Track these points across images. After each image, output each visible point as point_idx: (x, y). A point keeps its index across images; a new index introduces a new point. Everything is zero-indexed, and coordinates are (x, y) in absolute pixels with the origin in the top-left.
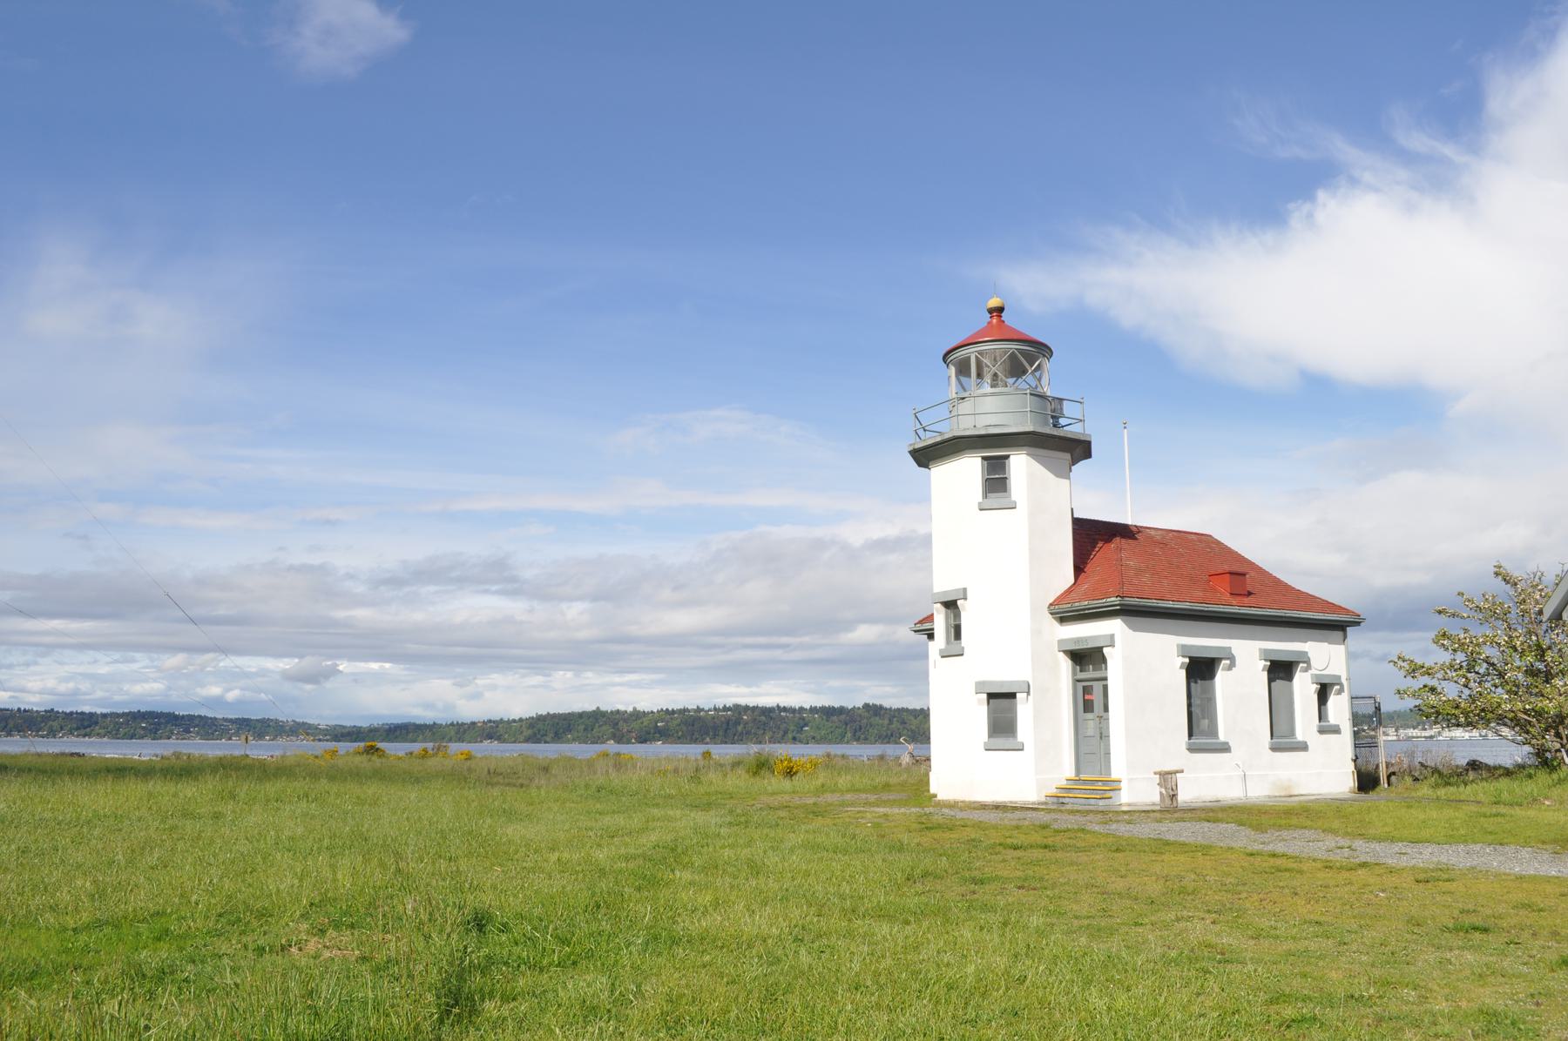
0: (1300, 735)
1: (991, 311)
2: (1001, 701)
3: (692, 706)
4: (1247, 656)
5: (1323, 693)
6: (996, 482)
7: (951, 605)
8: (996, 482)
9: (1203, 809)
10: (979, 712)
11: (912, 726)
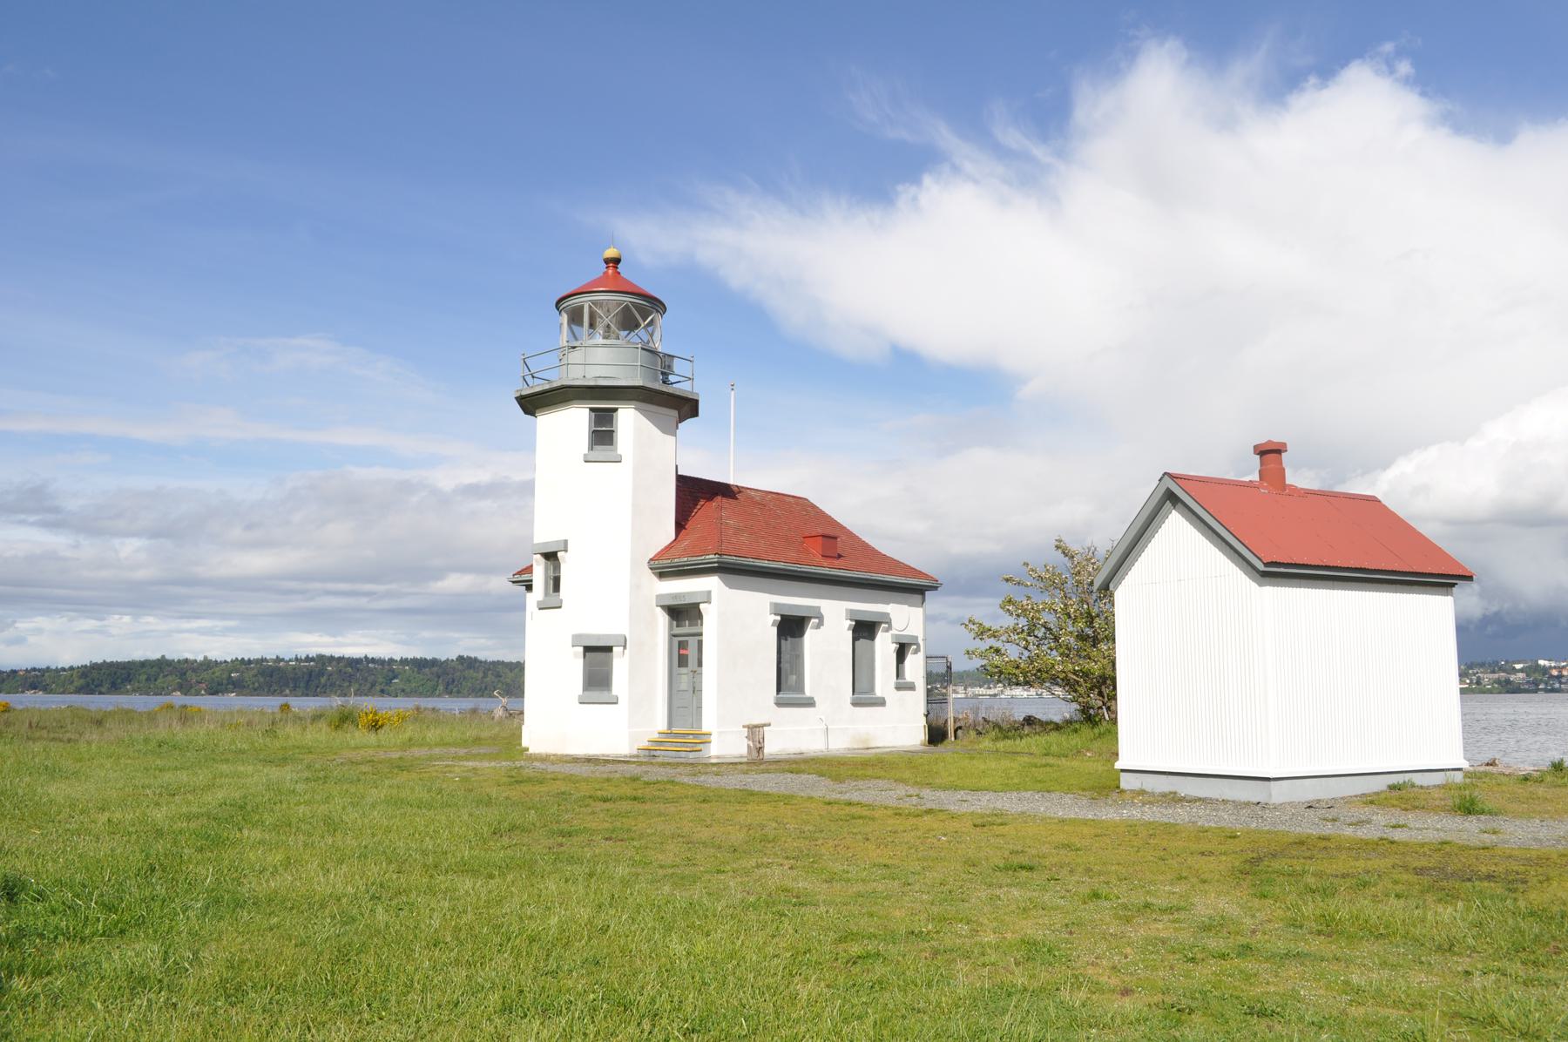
1: (607, 261)
2: (597, 654)
4: (834, 615)
6: (602, 435)
7: (551, 557)
8: (602, 435)
9: (787, 761)
11: (507, 679)
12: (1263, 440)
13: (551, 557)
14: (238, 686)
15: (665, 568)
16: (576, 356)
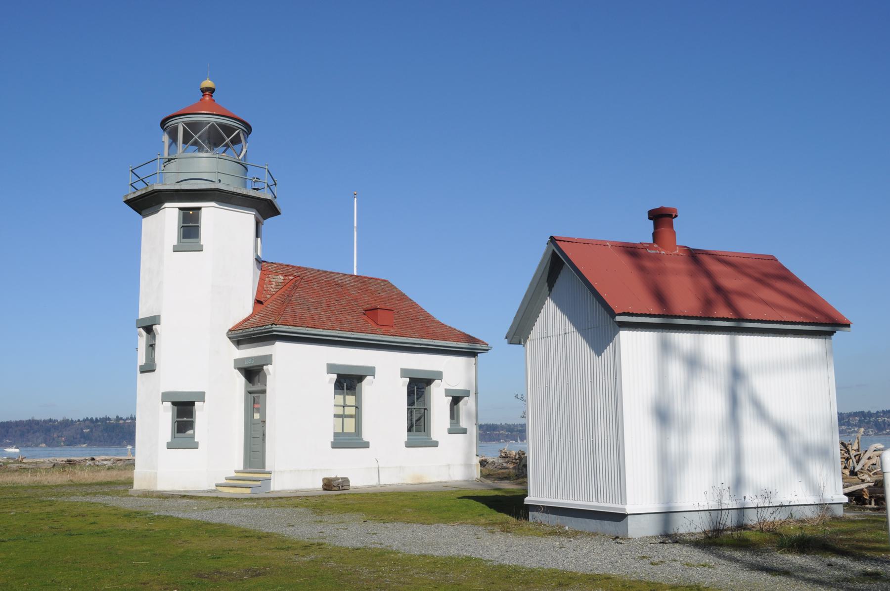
0: (434, 437)
1: (203, 90)
2: (184, 411)
3: (113, 416)
4: (387, 373)
5: (456, 400)
6: (190, 228)
7: (149, 330)
8: (190, 228)
9: (288, 498)
10: (166, 415)
11: (121, 432)
12: (656, 206)
13: (149, 330)
14: (87, 439)
15: (242, 336)
16: (172, 166)
